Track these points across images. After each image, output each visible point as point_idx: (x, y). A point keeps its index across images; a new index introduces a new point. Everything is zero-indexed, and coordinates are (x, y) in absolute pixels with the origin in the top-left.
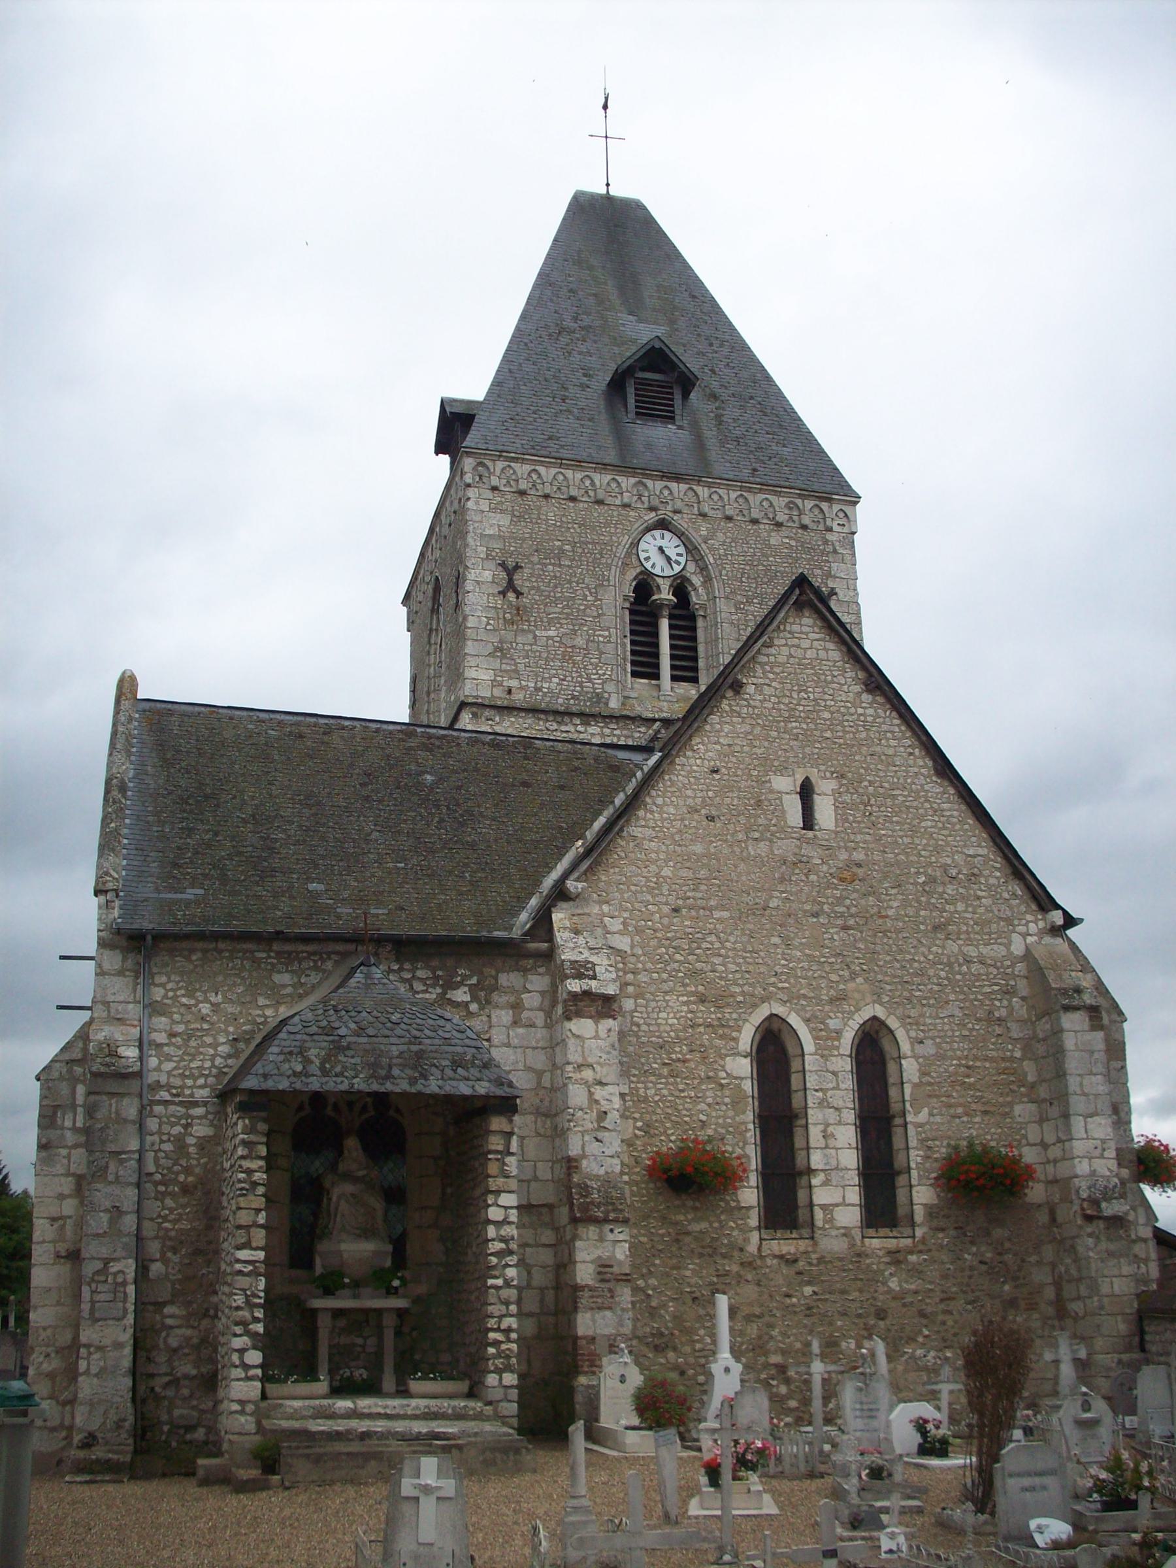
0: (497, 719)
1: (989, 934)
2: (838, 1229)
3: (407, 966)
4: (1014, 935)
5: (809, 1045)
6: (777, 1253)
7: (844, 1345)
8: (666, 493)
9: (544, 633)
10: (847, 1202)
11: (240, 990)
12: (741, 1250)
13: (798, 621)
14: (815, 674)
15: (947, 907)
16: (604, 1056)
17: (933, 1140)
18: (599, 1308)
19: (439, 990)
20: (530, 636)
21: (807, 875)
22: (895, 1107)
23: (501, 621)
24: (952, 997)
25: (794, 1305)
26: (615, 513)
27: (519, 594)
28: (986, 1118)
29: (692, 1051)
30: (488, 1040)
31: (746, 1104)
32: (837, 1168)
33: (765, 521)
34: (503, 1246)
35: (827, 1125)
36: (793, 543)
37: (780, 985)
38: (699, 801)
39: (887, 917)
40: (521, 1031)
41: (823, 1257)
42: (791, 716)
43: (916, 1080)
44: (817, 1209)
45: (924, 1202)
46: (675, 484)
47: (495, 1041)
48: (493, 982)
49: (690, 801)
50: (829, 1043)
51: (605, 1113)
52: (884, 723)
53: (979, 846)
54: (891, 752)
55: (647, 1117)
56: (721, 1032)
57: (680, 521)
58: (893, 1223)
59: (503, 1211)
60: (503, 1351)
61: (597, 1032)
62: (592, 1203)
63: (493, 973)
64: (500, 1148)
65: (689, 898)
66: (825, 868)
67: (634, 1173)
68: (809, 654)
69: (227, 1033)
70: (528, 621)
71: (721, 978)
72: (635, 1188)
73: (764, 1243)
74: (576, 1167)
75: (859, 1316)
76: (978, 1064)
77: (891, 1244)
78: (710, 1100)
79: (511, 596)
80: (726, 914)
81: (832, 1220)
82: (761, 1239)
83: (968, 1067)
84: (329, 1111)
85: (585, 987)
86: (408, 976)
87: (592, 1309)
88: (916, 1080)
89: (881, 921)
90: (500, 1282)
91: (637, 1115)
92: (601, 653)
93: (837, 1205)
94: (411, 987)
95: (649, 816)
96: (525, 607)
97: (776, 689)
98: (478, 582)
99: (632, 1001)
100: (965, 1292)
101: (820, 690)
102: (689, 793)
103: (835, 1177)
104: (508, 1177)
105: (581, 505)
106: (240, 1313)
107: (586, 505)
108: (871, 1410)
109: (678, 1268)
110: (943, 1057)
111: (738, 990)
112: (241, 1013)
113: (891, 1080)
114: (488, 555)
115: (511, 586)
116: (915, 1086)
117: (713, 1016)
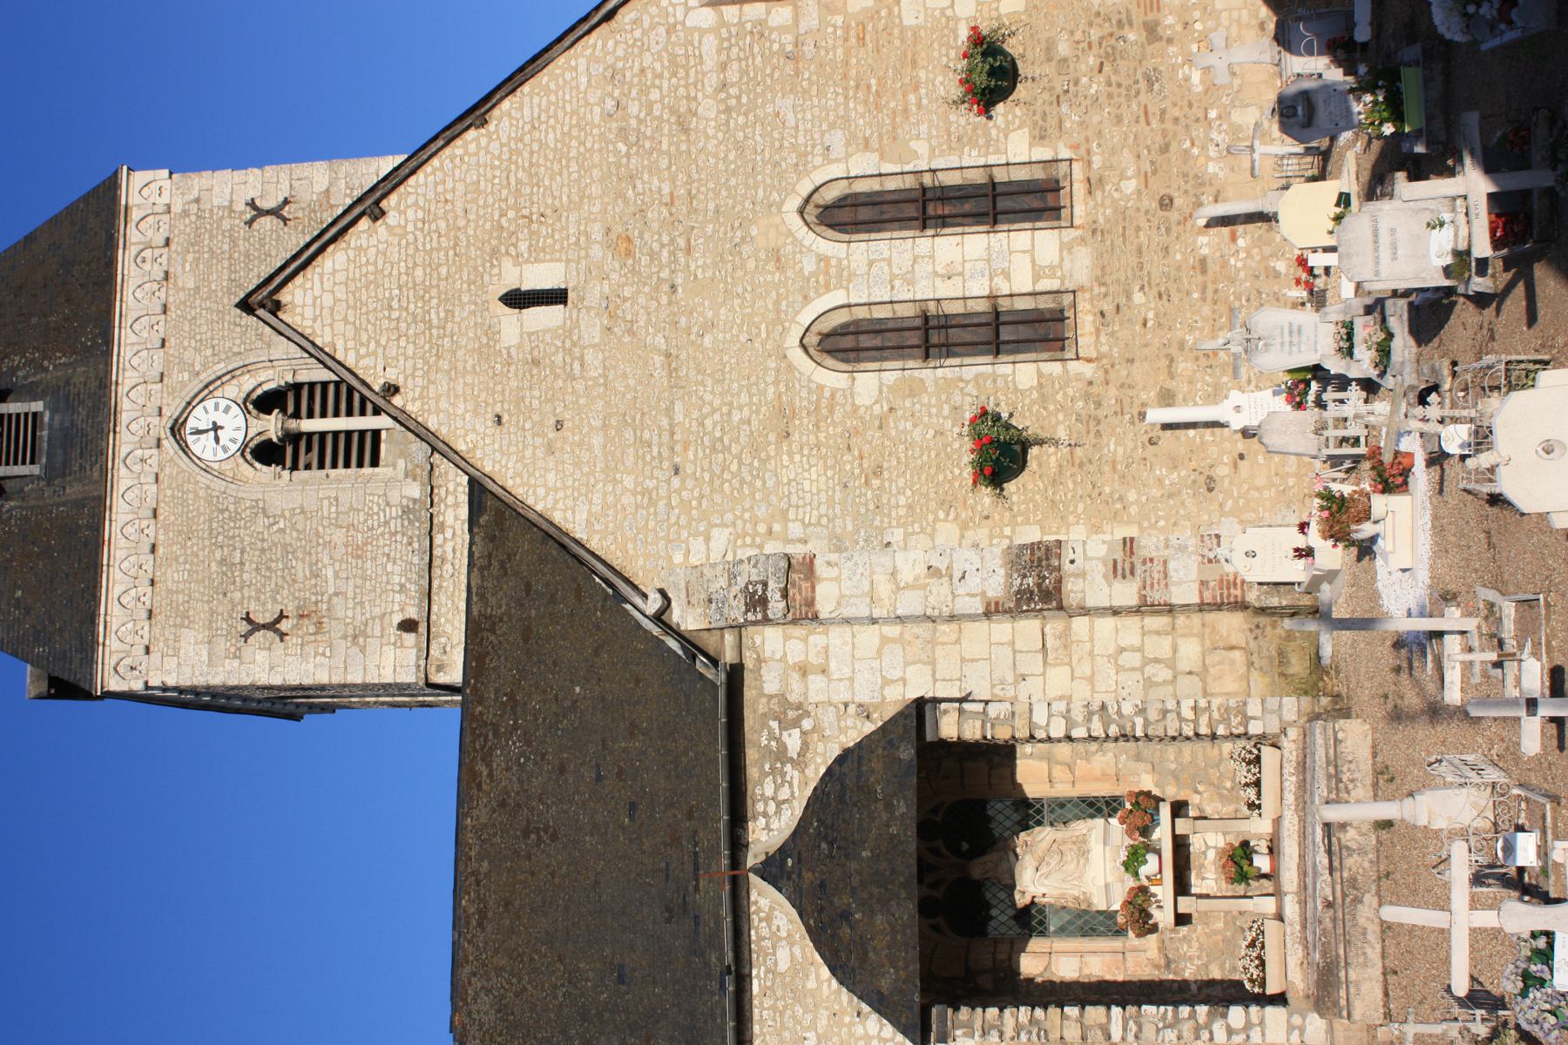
0: (443, 640)
1: (687, 56)
2: (1062, 260)
3: (760, 807)
4: (688, 23)
5: (837, 297)
6: (1094, 338)
7: (1205, 251)
8: (133, 427)
9: (331, 582)
10: (1029, 247)
11: (799, 1010)
12: (1090, 383)
13: (298, 310)
14: (367, 288)
15: (657, 113)
16: (861, 570)
17: (949, 135)
18: (1166, 577)
19: (788, 767)
20: (335, 600)
21: (625, 300)
22: (909, 182)
23: (319, 637)
24: (769, 109)
25: (1157, 316)
26: (169, 493)
27: (282, 616)
28: (921, 63)
29: (849, 448)
30: (846, 705)
31: (913, 379)
32: (988, 261)
33: (163, 296)
34: (1096, 718)
35: (936, 274)
36: (190, 257)
37: (764, 335)
38: (539, 441)
39: (672, 195)
40: (833, 665)
41: (1097, 279)
42: (423, 321)
43: (875, 157)
44: (1040, 287)
45: (1026, 146)
46: (124, 415)
47: (847, 697)
48: (775, 700)
49: (540, 453)
50: (833, 271)
51: (929, 568)
52: (425, 195)
53: (575, 69)
54: (460, 187)
55: (933, 505)
56: (824, 412)
57: (171, 412)
58: (1053, 187)
59: (1054, 719)
60: (1221, 715)
61: (831, 579)
62: (1039, 585)
63: (764, 700)
64: (978, 724)
65: (660, 453)
66: (614, 276)
67: (1001, 519)
68: (341, 295)
69: (851, 1024)
70: (316, 603)
71: (758, 412)
72: (1020, 519)
73: (1081, 355)
74: (997, 604)
75: (1168, 230)
76: (853, 73)
77: (1079, 189)
78: (909, 425)
79: (284, 626)
80: (678, 407)
81: (1052, 268)
82: (1078, 358)
83: (857, 87)
84: (939, 894)
85: (778, 596)
86: (772, 807)
87: (1166, 585)
88: (875, 157)
89: (677, 203)
90: (1139, 721)
91: (931, 517)
92: (351, 508)
93: (1033, 261)
94: (784, 801)
95: (560, 505)
96: (298, 608)
97: (389, 339)
98: (272, 668)
99: (790, 525)
100: (1138, 93)
101: (387, 280)
102: (528, 453)
103: (999, 264)
104: (1013, 713)
105: (161, 537)
106: (1185, 1034)
107: (161, 532)
108: (1291, 333)
109: (1114, 463)
110: (846, 118)
111: (771, 390)
112: (827, 1009)
113: (877, 187)
114: (235, 657)
115: (272, 626)
116: (882, 157)
117: (806, 421)
